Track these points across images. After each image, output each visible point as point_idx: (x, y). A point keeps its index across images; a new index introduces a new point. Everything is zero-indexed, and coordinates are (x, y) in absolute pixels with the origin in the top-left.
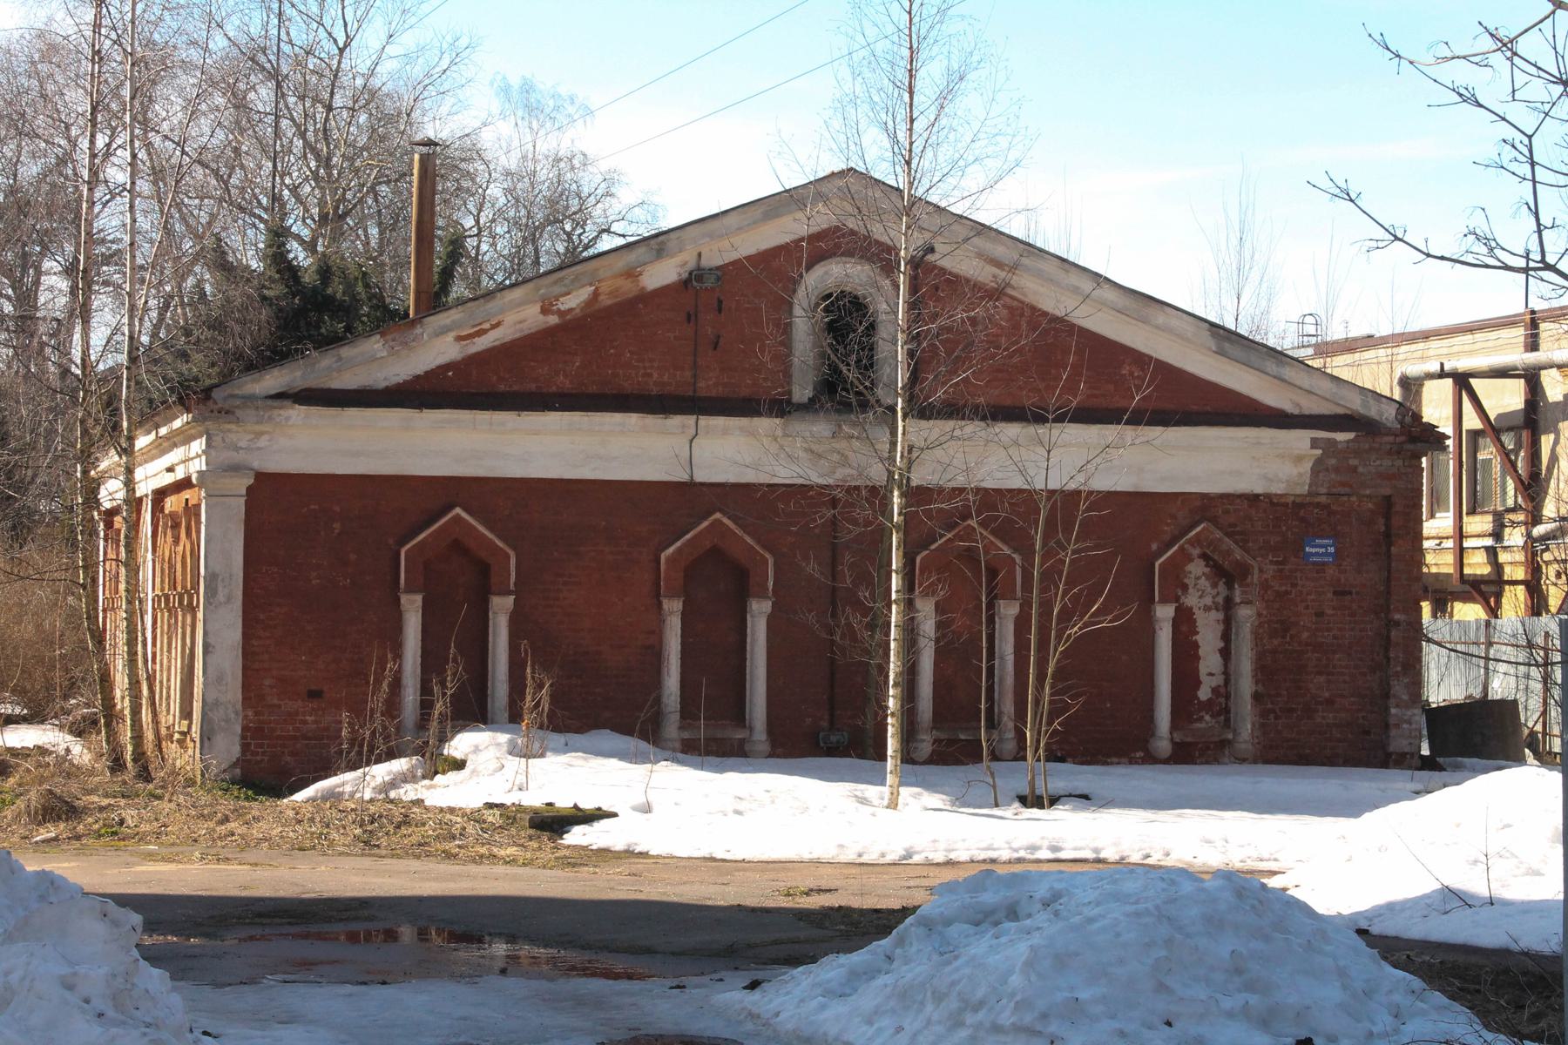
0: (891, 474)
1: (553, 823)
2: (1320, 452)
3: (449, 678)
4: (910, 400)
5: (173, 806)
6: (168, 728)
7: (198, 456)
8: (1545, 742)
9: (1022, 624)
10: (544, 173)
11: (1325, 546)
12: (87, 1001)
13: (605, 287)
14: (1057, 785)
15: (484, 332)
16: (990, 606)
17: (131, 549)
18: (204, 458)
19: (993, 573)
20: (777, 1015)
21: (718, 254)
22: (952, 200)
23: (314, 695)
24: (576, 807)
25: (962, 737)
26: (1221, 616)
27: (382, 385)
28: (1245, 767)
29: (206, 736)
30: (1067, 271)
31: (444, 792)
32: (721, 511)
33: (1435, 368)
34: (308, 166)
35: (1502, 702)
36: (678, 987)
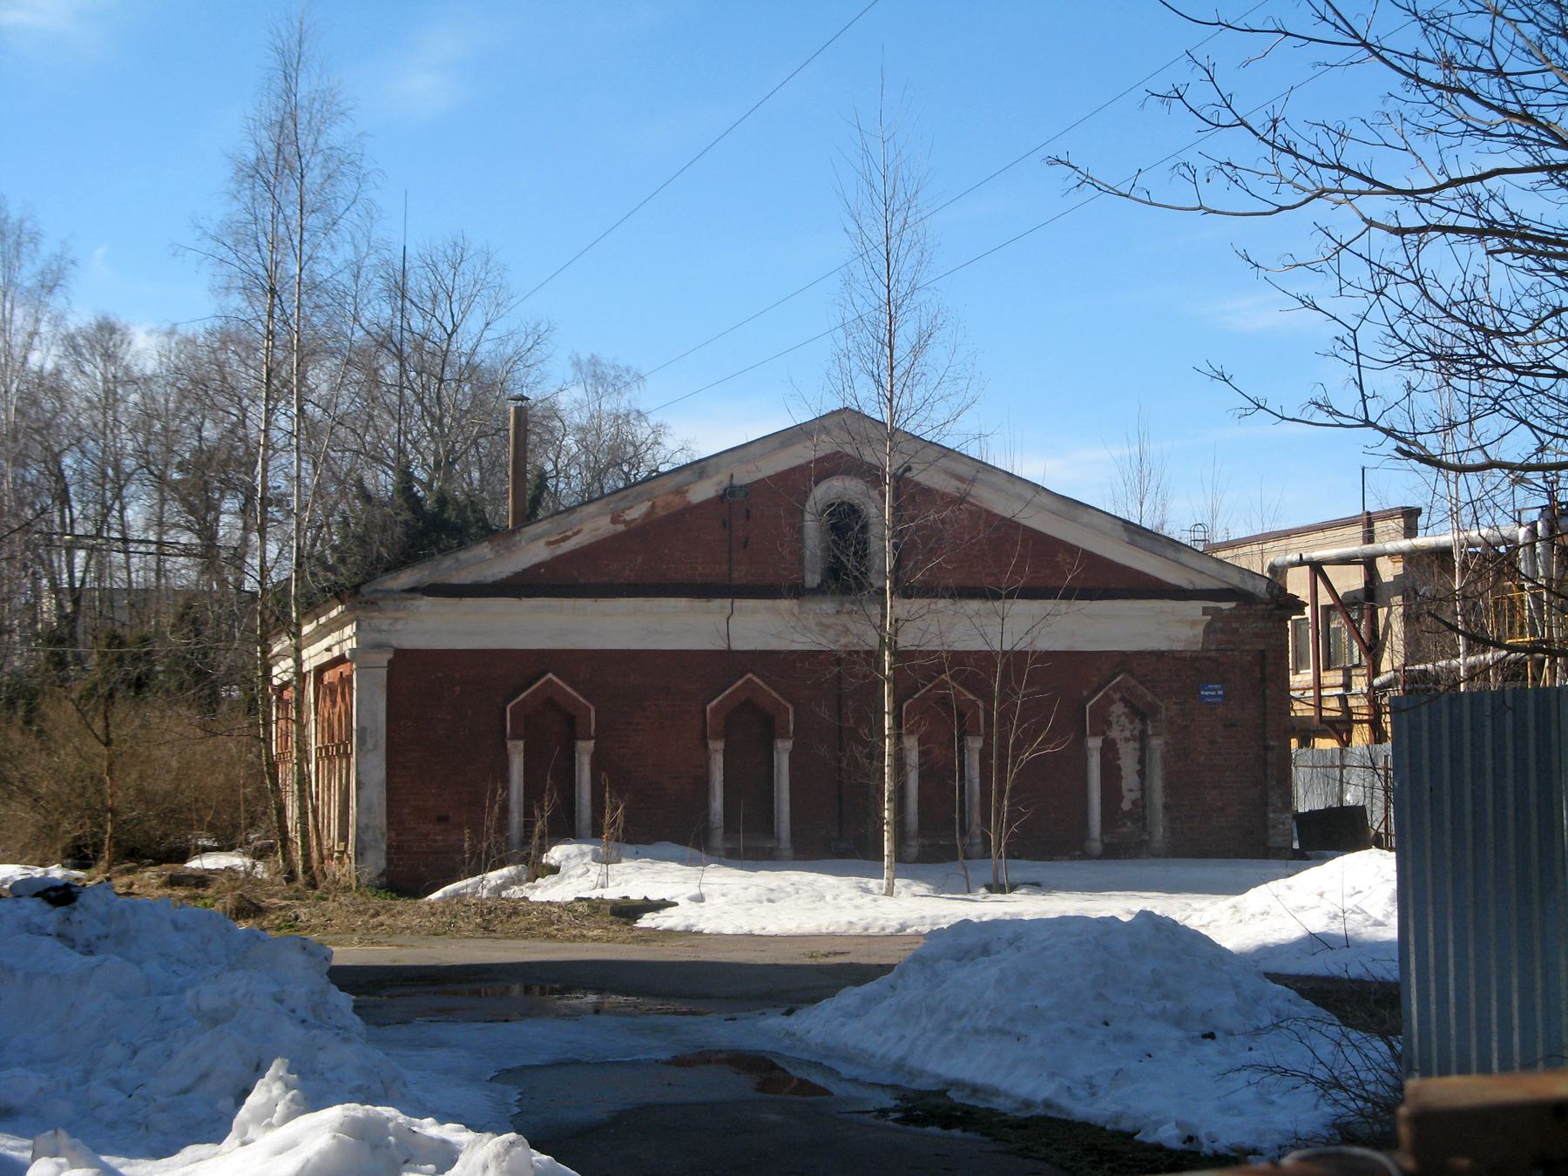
0: (882, 639)
1: (628, 911)
2: (1209, 618)
3: (546, 803)
4: (896, 583)
5: (336, 904)
6: (329, 849)
7: (350, 637)
8: (1387, 841)
9: (985, 755)
10: (608, 429)
11: (1216, 690)
12: (293, 1011)
13: (659, 502)
14: (1016, 876)
15: (567, 538)
16: (960, 740)
17: (299, 712)
18: (354, 639)
19: (961, 715)
20: (808, 1032)
21: (744, 477)
22: (925, 429)
23: (443, 819)
24: (646, 898)
25: (942, 843)
26: (1137, 745)
27: (490, 580)
28: (1159, 861)
29: (360, 854)
30: (1013, 483)
31: (546, 892)
32: (752, 672)
33: (1295, 557)
34: (426, 425)
35: (1355, 807)
36: (730, 1019)
